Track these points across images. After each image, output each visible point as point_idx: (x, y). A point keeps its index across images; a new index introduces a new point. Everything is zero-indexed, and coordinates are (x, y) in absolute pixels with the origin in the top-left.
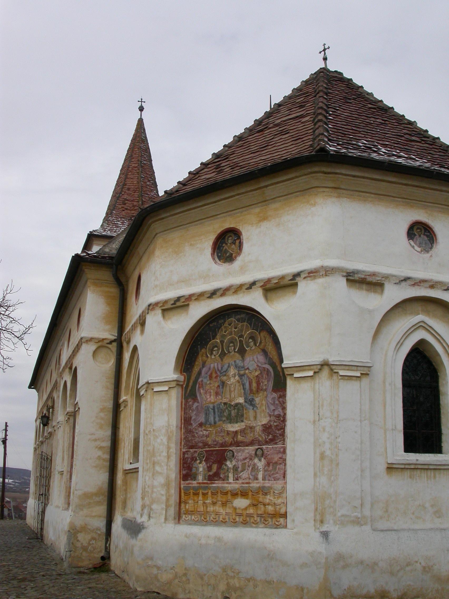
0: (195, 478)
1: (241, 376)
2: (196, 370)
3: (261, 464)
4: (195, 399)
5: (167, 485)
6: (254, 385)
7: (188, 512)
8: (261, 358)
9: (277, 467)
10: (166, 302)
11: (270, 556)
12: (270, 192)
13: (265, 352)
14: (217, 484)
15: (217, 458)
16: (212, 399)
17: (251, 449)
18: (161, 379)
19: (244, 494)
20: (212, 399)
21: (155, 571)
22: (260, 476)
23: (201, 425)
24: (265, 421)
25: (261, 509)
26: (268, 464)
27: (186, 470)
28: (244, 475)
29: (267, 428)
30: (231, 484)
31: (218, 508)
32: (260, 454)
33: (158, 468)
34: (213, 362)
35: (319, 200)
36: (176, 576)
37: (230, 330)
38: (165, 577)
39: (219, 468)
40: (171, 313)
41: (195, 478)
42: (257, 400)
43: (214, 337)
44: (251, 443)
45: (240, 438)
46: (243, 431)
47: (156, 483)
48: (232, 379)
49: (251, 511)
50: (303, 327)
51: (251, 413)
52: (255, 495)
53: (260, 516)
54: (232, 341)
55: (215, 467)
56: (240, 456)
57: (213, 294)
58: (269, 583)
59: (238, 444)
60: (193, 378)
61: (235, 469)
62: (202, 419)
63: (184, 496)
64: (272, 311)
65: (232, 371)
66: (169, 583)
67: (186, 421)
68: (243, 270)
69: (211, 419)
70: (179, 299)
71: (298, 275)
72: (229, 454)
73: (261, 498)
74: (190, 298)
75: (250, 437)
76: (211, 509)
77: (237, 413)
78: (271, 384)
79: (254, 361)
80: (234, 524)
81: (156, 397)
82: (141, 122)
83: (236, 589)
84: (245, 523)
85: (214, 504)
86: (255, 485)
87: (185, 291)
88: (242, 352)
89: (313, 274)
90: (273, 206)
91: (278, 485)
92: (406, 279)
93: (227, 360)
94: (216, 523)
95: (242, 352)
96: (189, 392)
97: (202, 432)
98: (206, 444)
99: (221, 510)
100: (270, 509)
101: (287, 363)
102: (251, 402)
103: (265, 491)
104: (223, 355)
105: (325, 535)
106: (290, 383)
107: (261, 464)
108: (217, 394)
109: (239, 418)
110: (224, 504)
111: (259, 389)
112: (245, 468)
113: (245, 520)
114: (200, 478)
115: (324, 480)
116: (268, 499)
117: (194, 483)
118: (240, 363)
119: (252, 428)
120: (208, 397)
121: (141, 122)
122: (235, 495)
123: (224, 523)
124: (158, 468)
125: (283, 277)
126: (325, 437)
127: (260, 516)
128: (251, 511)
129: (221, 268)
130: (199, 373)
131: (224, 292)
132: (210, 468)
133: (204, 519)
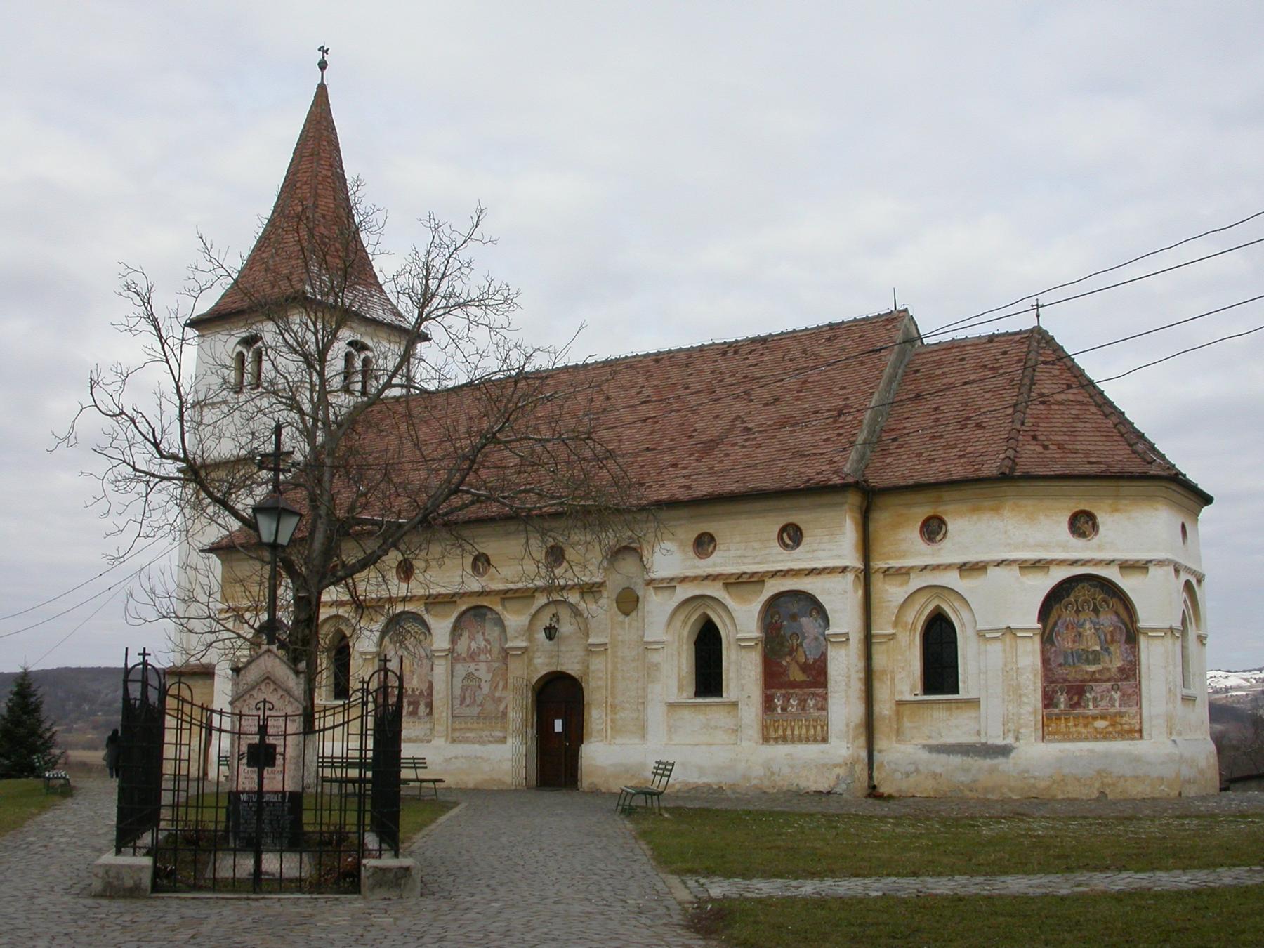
0: (1056, 706)
1: (1096, 630)
2: (1052, 620)
3: (1117, 696)
4: (1052, 643)
5: (1035, 712)
6: (1109, 637)
7: (1050, 733)
8: (1115, 618)
9: (1134, 697)
10: (1026, 561)
11: (1136, 759)
13: (1117, 614)
15: (1078, 692)
16: (1070, 645)
17: (1109, 685)
18: (1027, 626)
19: (1103, 717)
20: (1070, 645)
21: (1032, 781)
22: (1117, 704)
23: (1060, 665)
24: (1119, 665)
25: (1119, 728)
26: (1123, 695)
27: (1049, 700)
28: (1103, 703)
29: (1121, 670)
31: (1080, 729)
32: (1116, 688)
33: (1024, 699)
34: (1068, 616)
35: (1159, 506)
36: (1054, 782)
38: (1042, 785)
40: (1026, 571)
41: (1056, 706)
42: (1112, 649)
43: (1068, 596)
44: (1109, 680)
46: (1100, 671)
47: (1023, 711)
48: (1088, 629)
51: (1107, 658)
52: (1114, 719)
53: (1118, 732)
54: (1085, 601)
56: (1098, 689)
57: (1074, 563)
58: (1137, 777)
59: (1096, 681)
61: (1095, 699)
62: (1061, 661)
63: (1047, 721)
64: (1128, 583)
65: (1088, 625)
66: (1048, 788)
67: (1045, 661)
69: (1070, 661)
70: (1039, 561)
71: (1150, 561)
73: (1118, 719)
74: (1051, 562)
75: (1107, 675)
76: (1073, 729)
77: (1095, 658)
78: (1123, 638)
79: (1107, 619)
80: (1096, 739)
81: (1019, 641)
82: (322, 90)
83: (1109, 785)
84: (1105, 738)
85: (1076, 725)
86: (1112, 710)
88: (1096, 611)
89: (1160, 563)
90: (1124, 502)
91: (1133, 710)
93: (1082, 617)
94: (1079, 739)
95: (1096, 611)
96: (1047, 638)
97: (1060, 671)
98: (1065, 680)
99: (1083, 730)
100: (1126, 727)
101: (1141, 624)
102: (1107, 650)
103: (1121, 715)
104: (1078, 612)
105: (1174, 741)
106: (1143, 641)
107: (1117, 696)
108: (1074, 642)
110: (1085, 726)
111: (1113, 641)
112: (1102, 698)
113: (1105, 736)
114: (1062, 707)
115: (1171, 706)
116: (1124, 720)
117: (1056, 711)
118: (1095, 620)
119: (1108, 669)
120: (1066, 642)
121: (322, 90)
122: (1095, 718)
123: (1086, 739)
124: (1024, 699)
125: (1138, 561)
126: (1171, 678)
127: (1118, 732)
129: (1080, 542)
130: (1055, 624)
131: (1085, 563)
132: (1071, 699)
133: (1067, 737)
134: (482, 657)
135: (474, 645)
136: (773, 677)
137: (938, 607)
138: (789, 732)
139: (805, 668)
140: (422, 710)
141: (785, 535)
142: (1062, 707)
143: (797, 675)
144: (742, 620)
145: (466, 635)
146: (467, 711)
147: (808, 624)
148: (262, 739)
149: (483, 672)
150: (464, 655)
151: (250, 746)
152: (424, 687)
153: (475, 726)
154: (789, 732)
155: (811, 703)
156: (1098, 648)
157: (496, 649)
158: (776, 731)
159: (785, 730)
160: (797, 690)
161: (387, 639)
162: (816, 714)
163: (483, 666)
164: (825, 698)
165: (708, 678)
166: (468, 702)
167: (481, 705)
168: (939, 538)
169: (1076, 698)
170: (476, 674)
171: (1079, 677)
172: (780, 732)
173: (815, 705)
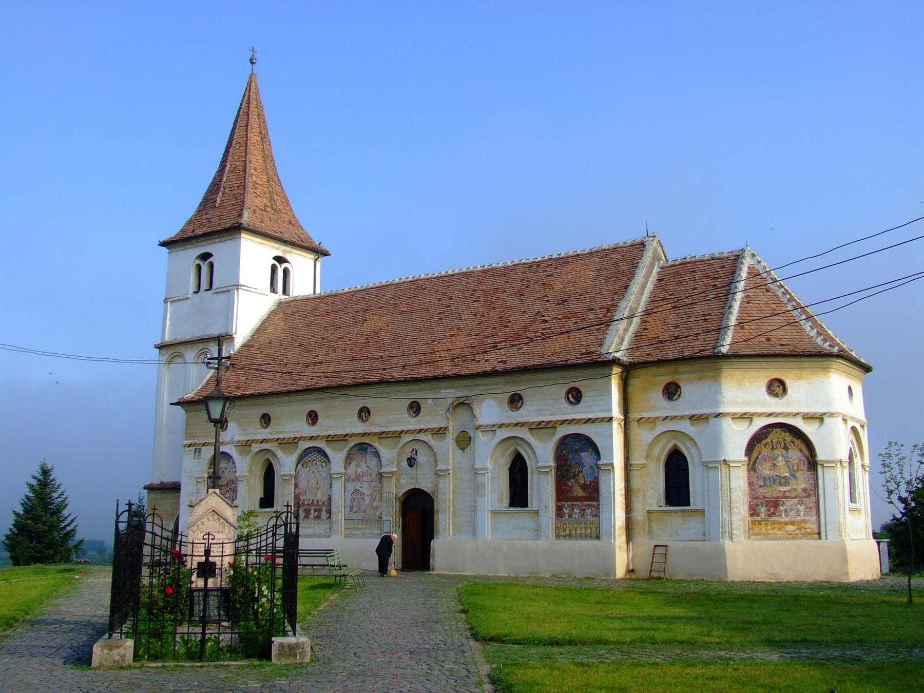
6: (795, 467)
7: (754, 534)
10: (736, 414)
12: (805, 364)
14: (774, 518)
15: (774, 505)
16: (768, 472)
17: (796, 500)
19: (792, 523)
20: (768, 472)
22: (802, 514)
24: (803, 486)
27: (753, 512)
28: (791, 513)
30: (784, 518)
37: (776, 436)
39: (776, 509)
41: (758, 515)
42: (798, 475)
44: (795, 497)
45: (787, 494)
46: (789, 491)
48: (780, 462)
49: (797, 532)
50: (833, 442)
55: (772, 510)
57: (770, 415)
59: (786, 497)
60: (753, 459)
61: (786, 511)
65: (780, 458)
68: (788, 404)
69: (768, 483)
72: (780, 503)
75: (794, 494)
76: (771, 532)
80: (788, 539)
84: (793, 538)
86: (799, 519)
87: (752, 410)
92: (667, 418)
93: (776, 452)
95: (786, 448)
96: (752, 467)
98: (765, 497)
100: (809, 530)
102: (794, 476)
104: (773, 449)
107: (802, 508)
109: (786, 483)
110: (779, 529)
112: (792, 510)
114: (763, 516)
116: (807, 525)
117: (759, 518)
118: (785, 454)
120: (765, 470)
122: (786, 524)
125: (815, 414)
128: (797, 532)
132: (769, 510)
134: (365, 479)
135: (359, 470)
136: (562, 493)
137: (675, 445)
138: (573, 532)
139: (584, 487)
140: (324, 515)
141: (570, 395)
142: (763, 516)
143: (580, 493)
144: (542, 454)
145: (354, 462)
146: (355, 516)
147: (587, 457)
148: (207, 559)
149: (365, 489)
150: (353, 477)
151: (199, 563)
152: (326, 499)
153: (360, 526)
154: (573, 532)
155: (588, 511)
156: (788, 475)
157: (374, 473)
158: (564, 531)
159: (571, 530)
160: (578, 503)
161: (300, 465)
162: (592, 519)
163: (365, 485)
164: (598, 508)
165: (519, 495)
166: (355, 509)
167: (364, 511)
168: (675, 397)
169: (772, 510)
170: (361, 490)
171: (774, 495)
172: (568, 532)
173: (591, 513)
